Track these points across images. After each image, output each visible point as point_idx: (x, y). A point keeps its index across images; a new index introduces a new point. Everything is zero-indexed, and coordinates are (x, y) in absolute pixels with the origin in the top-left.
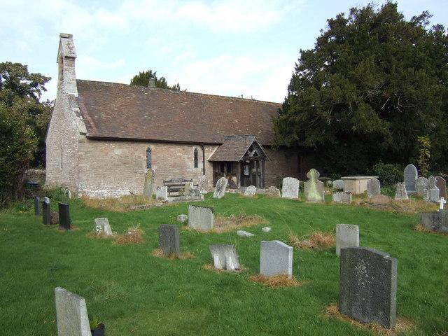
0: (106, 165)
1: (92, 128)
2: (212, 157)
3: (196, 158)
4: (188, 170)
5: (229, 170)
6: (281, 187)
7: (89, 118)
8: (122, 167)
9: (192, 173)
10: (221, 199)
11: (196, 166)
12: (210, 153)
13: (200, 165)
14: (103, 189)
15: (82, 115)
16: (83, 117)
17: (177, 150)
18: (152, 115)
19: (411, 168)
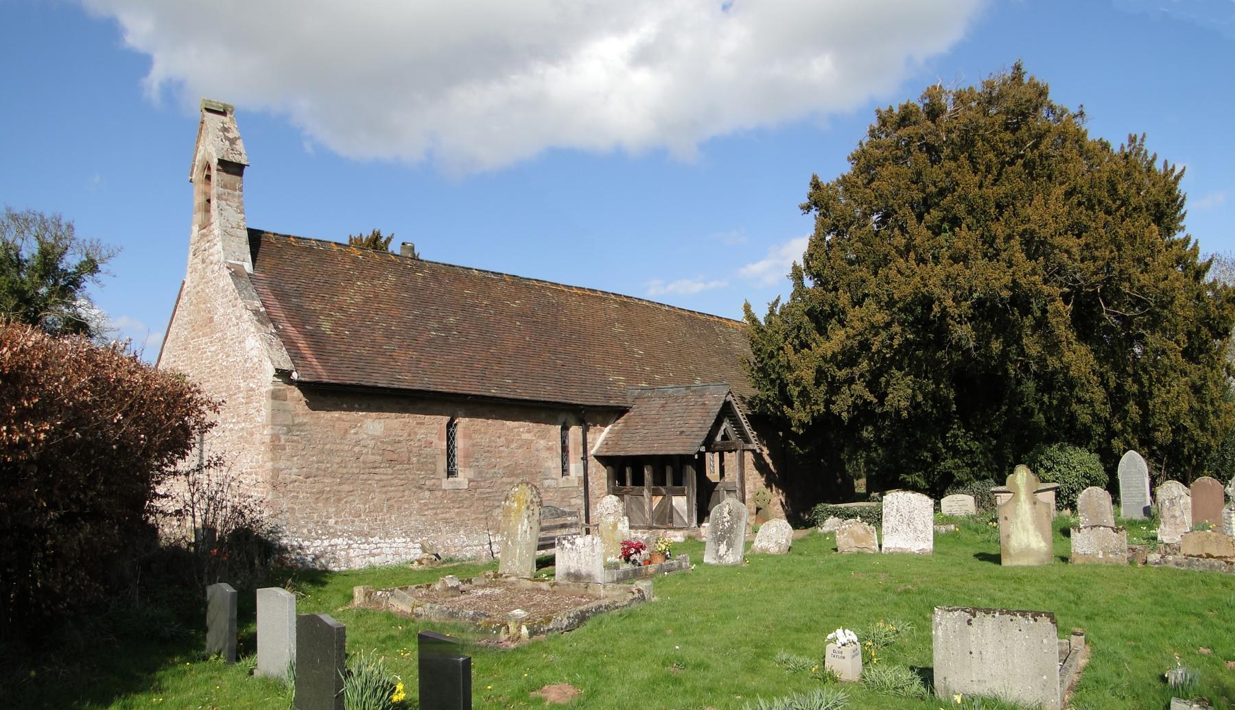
0: (342, 463)
1: (303, 358)
2: (606, 443)
3: (565, 449)
4: (547, 483)
5: (659, 481)
6: (880, 520)
7: (291, 331)
8: (386, 472)
9: (557, 489)
10: (686, 541)
11: (565, 471)
12: (600, 438)
13: (575, 468)
14: (334, 535)
15: (272, 321)
16: (276, 328)
17: (523, 430)
18: (446, 329)
19: (925, 540)
